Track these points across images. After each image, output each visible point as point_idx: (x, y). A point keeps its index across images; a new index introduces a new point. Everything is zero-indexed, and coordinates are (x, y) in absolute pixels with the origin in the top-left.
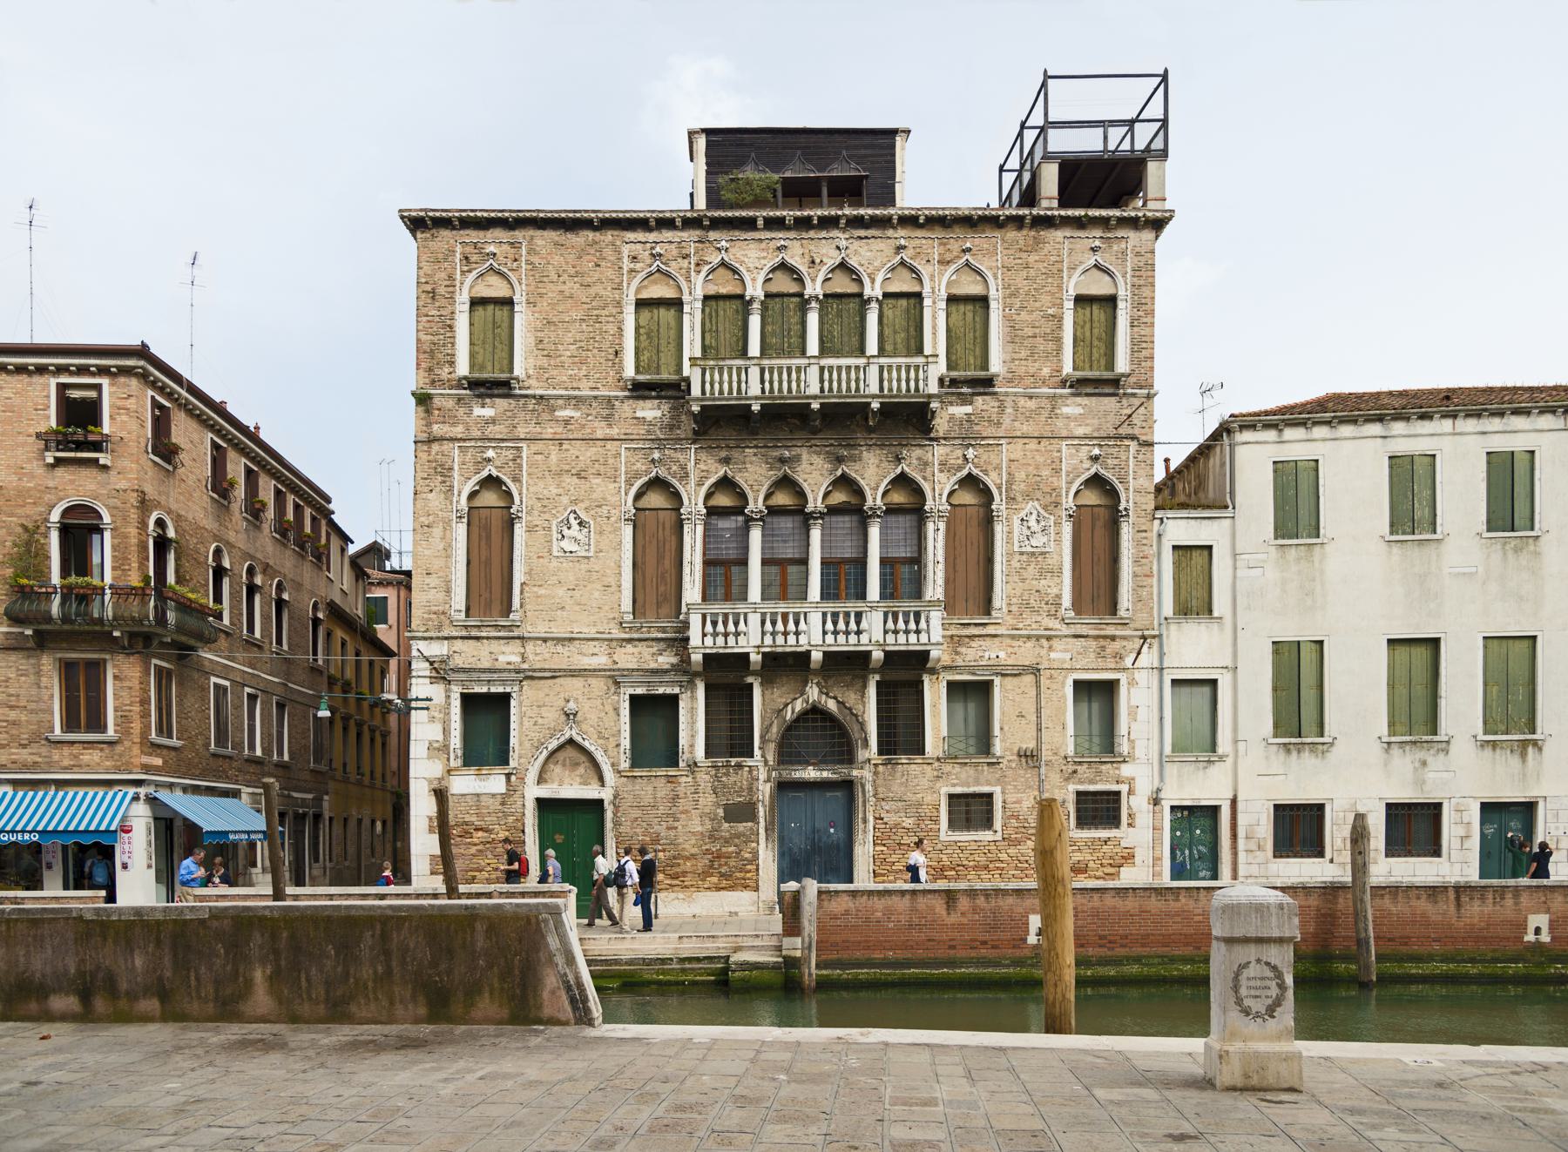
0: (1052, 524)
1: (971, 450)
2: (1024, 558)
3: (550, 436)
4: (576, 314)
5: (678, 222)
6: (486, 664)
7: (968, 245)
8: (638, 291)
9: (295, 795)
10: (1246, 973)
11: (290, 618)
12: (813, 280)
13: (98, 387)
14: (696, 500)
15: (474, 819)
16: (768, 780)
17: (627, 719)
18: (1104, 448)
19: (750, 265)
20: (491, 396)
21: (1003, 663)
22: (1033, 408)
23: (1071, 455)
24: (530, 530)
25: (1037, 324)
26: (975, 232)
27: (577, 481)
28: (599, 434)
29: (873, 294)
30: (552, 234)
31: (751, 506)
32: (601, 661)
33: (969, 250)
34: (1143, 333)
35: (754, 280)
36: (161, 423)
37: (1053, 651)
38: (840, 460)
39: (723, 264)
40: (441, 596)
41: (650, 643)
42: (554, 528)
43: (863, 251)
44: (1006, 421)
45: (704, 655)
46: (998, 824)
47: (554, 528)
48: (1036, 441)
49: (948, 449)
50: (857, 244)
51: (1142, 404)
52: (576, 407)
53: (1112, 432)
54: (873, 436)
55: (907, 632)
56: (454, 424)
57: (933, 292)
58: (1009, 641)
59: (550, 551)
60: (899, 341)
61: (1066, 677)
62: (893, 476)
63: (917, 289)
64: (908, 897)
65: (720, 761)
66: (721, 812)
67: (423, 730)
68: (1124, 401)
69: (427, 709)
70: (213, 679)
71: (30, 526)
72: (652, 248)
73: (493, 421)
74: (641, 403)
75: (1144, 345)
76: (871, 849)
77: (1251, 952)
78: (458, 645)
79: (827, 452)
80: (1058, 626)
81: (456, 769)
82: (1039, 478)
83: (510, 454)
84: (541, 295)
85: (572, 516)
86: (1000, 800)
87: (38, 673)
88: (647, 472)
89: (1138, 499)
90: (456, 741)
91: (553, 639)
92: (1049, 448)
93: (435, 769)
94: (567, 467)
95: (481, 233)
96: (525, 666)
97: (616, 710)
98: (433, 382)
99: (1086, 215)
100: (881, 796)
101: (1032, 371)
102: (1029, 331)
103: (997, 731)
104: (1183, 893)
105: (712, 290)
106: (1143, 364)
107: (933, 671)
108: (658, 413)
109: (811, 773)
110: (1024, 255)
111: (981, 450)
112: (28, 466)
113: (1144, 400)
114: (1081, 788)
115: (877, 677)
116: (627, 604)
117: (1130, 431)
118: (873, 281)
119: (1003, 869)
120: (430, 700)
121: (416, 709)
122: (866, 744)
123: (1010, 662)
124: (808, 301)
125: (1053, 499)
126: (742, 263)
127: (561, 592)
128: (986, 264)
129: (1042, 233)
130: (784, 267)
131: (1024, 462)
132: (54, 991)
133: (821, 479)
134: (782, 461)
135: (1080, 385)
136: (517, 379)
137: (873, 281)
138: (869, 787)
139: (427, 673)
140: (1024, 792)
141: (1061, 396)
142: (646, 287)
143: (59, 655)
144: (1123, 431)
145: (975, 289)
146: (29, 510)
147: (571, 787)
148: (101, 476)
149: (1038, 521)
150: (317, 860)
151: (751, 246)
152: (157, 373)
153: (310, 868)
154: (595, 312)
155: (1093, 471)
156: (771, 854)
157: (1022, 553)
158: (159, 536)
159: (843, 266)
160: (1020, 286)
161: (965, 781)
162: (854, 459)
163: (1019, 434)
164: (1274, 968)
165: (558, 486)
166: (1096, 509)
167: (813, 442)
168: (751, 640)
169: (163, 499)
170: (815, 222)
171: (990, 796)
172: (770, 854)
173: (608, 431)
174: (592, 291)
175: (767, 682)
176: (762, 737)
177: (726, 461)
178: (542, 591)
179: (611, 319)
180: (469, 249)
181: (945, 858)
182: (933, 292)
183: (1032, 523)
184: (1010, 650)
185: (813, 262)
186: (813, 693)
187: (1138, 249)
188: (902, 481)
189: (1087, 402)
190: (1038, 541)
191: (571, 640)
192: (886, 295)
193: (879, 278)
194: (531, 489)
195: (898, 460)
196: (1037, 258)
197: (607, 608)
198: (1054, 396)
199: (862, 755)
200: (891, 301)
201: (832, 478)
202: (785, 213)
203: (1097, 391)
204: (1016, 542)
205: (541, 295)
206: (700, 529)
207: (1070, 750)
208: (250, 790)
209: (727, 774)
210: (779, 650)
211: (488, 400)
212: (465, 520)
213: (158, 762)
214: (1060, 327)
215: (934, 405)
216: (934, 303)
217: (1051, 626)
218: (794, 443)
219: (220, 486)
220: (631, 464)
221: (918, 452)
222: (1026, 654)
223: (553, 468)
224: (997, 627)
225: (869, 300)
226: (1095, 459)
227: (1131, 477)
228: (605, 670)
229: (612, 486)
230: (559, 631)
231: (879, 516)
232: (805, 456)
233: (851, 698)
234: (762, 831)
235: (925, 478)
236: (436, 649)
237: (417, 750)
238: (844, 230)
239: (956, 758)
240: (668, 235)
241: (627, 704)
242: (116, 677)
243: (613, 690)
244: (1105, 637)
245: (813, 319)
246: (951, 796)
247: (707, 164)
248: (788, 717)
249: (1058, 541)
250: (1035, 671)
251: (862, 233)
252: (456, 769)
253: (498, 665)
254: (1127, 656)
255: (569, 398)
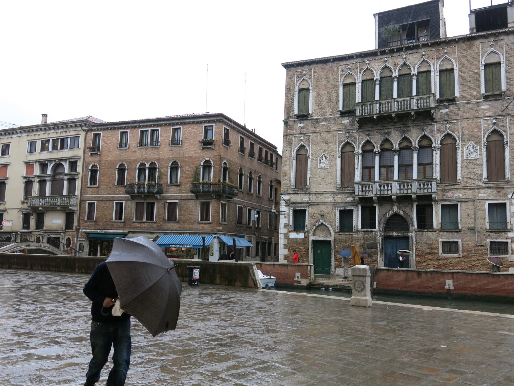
0: (478, 149)
1: (448, 125)
2: (468, 161)
3: (318, 131)
4: (326, 91)
5: (355, 57)
6: (299, 201)
7: (446, 51)
8: (343, 82)
9: (262, 237)
10: (357, 283)
11: (263, 186)
12: (395, 71)
13: (212, 126)
14: (359, 148)
15: (295, 245)
16: (381, 236)
17: (338, 217)
18: (497, 120)
19: (376, 68)
20: (303, 120)
21: (461, 198)
22: (470, 107)
23: (485, 124)
24: (312, 161)
25: (471, 77)
26: (449, 46)
27: (325, 145)
28: (331, 129)
29: (414, 73)
30: (320, 65)
31: (376, 149)
32: (331, 200)
33: (446, 53)
34: (511, 75)
35: (377, 73)
36: (227, 135)
37: (480, 193)
38: (404, 132)
39: (368, 69)
40: (288, 182)
41: (345, 194)
42: (318, 160)
43: (411, 58)
44: (461, 113)
45: (359, 198)
46: (460, 251)
47: (318, 160)
48: (471, 119)
49: (440, 125)
50: (409, 56)
51: (512, 102)
52: (325, 122)
53: (500, 113)
54: (415, 122)
55: (424, 189)
56: (293, 130)
57: (434, 70)
58: (463, 190)
59: (317, 167)
60: (424, 88)
61: (485, 202)
62: (421, 136)
63: (429, 69)
64: (405, 272)
65: (365, 230)
66: (366, 245)
67: (283, 220)
68: (505, 102)
69: (284, 214)
70: (238, 205)
71: (197, 166)
72: (348, 66)
73: (303, 128)
74: (343, 118)
75: (511, 79)
76: (415, 259)
77: (358, 278)
78: (293, 196)
79: (400, 130)
80: (482, 185)
81: (291, 231)
82: (473, 133)
83: (307, 138)
84: (317, 86)
85: (323, 156)
86: (461, 244)
87: (196, 206)
88: (345, 140)
89: (511, 137)
90: (291, 223)
91: (318, 193)
92: (477, 121)
93: (285, 231)
94: (322, 141)
95: (302, 67)
96: (310, 202)
97: (335, 214)
98: (288, 117)
99: (487, 34)
100: (418, 241)
101: (470, 94)
102: (468, 80)
103: (459, 221)
104: (501, 276)
105: (365, 78)
106: (511, 87)
107: (436, 201)
108: (348, 121)
109: (395, 234)
110: (466, 52)
111: (452, 125)
112: (197, 150)
113: (512, 100)
114: (492, 240)
115: (416, 203)
116: (338, 182)
117: (507, 112)
118: (414, 69)
119: (462, 266)
120: (285, 212)
121: (281, 214)
122: (413, 225)
123: (464, 197)
124: (394, 78)
125: (479, 140)
126: (373, 68)
127: (320, 179)
128: (453, 57)
129: (472, 42)
130: (386, 67)
131: (468, 127)
132: (197, 280)
133: (398, 139)
134: (385, 134)
135: (486, 98)
136: (309, 114)
137: (414, 69)
138: (414, 239)
139: (284, 204)
140: (470, 241)
141: (481, 102)
142: (346, 80)
143: (201, 201)
144: (504, 113)
145: (449, 67)
146: (197, 162)
147: (321, 237)
148: (212, 151)
149: (473, 148)
150: (269, 255)
151: (376, 62)
152: (225, 120)
153: (267, 257)
154: (331, 90)
155: (493, 128)
156: (382, 258)
157: (467, 160)
158: (224, 167)
159: (405, 64)
160: (464, 63)
161: (447, 237)
162: (408, 131)
163: (465, 117)
164: (362, 282)
165: (320, 147)
166: (496, 142)
167: (395, 126)
168: (374, 191)
169: (226, 157)
170: (395, 50)
171: (457, 242)
172: (381, 258)
173: (334, 128)
174: (330, 83)
175: (380, 205)
176: (379, 222)
177: (368, 135)
178: (315, 179)
179: (336, 92)
180: (299, 73)
181: (441, 262)
182: (434, 70)
183: (471, 149)
184: (463, 193)
185: (395, 64)
186: (395, 209)
187: (508, 43)
188: (425, 137)
189: (490, 103)
190: (473, 155)
191: (322, 193)
192: (419, 73)
193: (416, 67)
194: (313, 148)
195: (423, 130)
196: (470, 52)
197: (333, 184)
198: (478, 102)
199: (412, 228)
200: (421, 74)
201: (401, 138)
202: (385, 49)
203: (494, 99)
204: (465, 156)
205: (317, 86)
206: (360, 158)
207: (488, 227)
208: (248, 235)
209: (368, 234)
210: (382, 196)
211: (302, 121)
212: (295, 159)
213: (221, 228)
214: (479, 77)
215: (433, 111)
216: (435, 73)
217: (479, 184)
218: (389, 127)
219: (242, 149)
220: (339, 138)
221: (430, 127)
222: (470, 194)
223: (319, 141)
224: (458, 186)
225: (413, 75)
226: (494, 124)
227: (508, 129)
228: (332, 202)
229: (335, 146)
230: (319, 190)
231: (417, 150)
232: (393, 131)
233: (408, 210)
234: (379, 251)
235: (432, 136)
236: (286, 197)
237: (281, 226)
238: (405, 51)
239: (444, 230)
240: (352, 61)
241: (338, 213)
242: (212, 206)
243: (334, 208)
244: (500, 188)
245: (395, 84)
246: (443, 243)
247: (378, 24)
248: (387, 217)
249: (481, 154)
250: (473, 200)
251: (411, 52)
252: (291, 231)
253: (303, 201)
254: (509, 194)
255: (323, 119)
